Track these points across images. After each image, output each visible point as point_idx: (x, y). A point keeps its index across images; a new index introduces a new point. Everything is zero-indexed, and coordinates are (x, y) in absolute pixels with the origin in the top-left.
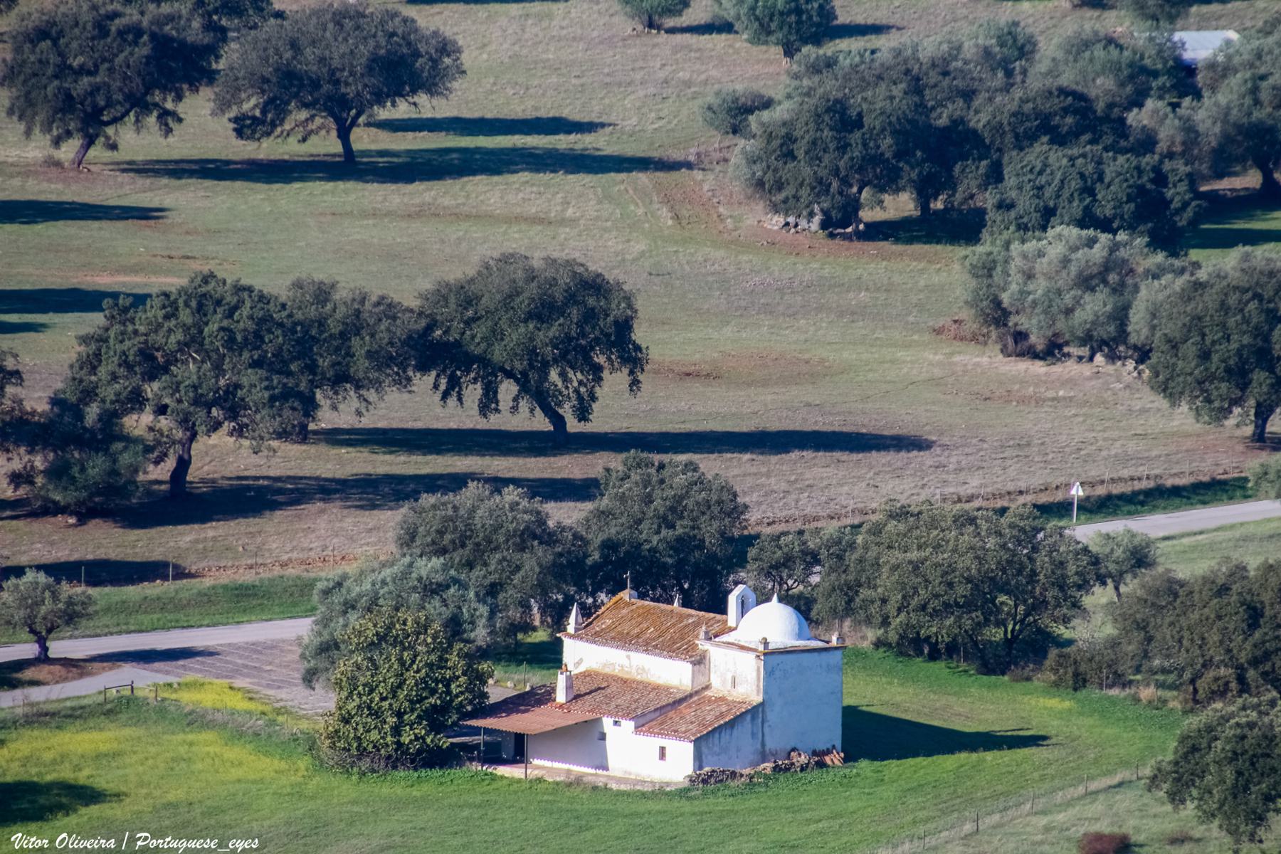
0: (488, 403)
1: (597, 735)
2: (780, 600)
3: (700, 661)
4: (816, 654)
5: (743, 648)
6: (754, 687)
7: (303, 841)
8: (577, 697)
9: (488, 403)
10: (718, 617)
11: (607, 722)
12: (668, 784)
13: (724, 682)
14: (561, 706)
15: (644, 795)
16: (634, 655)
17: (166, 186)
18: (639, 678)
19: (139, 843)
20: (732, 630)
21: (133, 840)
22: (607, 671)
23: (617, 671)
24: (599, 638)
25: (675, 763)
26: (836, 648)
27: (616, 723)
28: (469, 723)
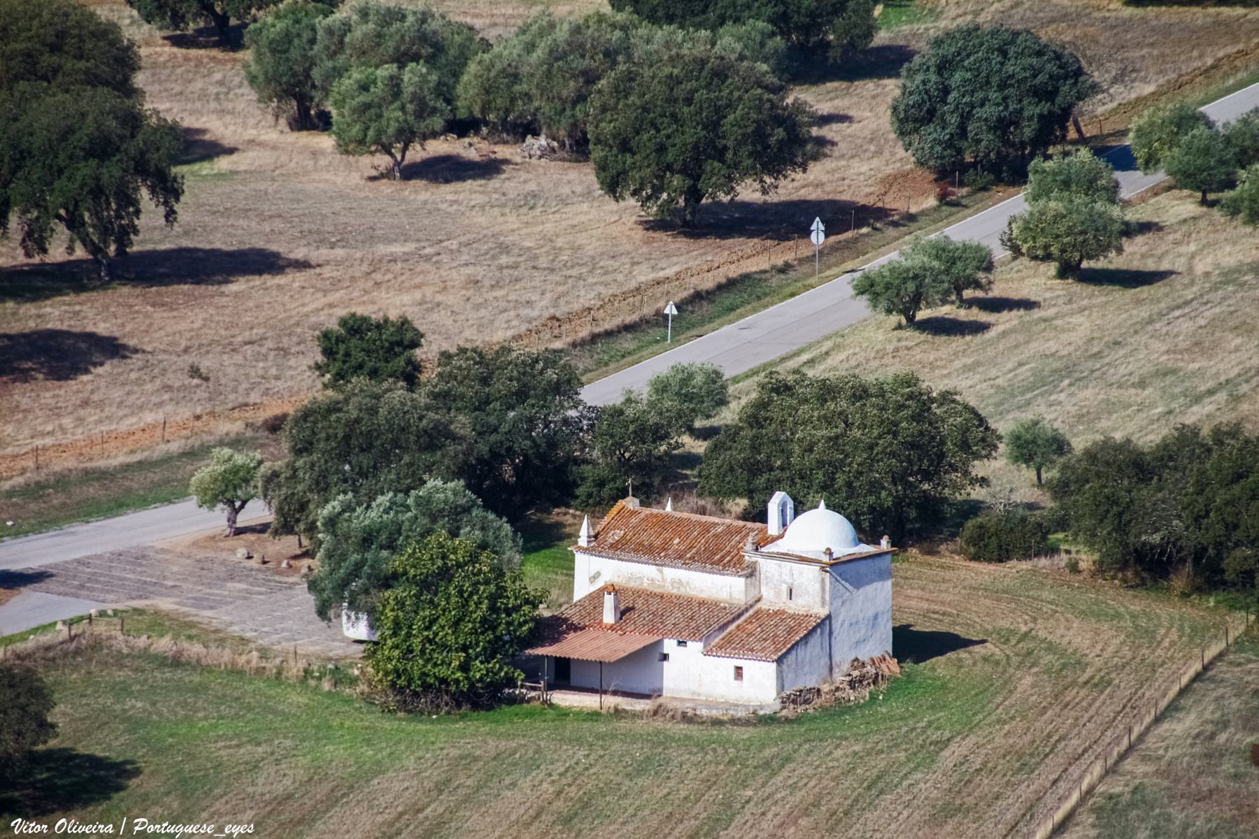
0: (35, 239)
1: (658, 656)
2: (828, 507)
3: (751, 573)
4: (864, 562)
5: (803, 560)
6: (818, 599)
7: (223, 800)
8: (623, 613)
9: (35, 239)
10: (759, 525)
11: (669, 646)
12: (762, 707)
13: (778, 594)
14: (612, 628)
15: (734, 721)
16: (666, 570)
17: (836, 89)
18: (675, 591)
19: (137, 828)
20: (774, 539)
21: (130, 826)
22: (632, 584)
23: (646, 585)
24: (617, 549)
25: (759, 684)
26: (887, 553)
27: (680, 643)
28: (540, 651)
